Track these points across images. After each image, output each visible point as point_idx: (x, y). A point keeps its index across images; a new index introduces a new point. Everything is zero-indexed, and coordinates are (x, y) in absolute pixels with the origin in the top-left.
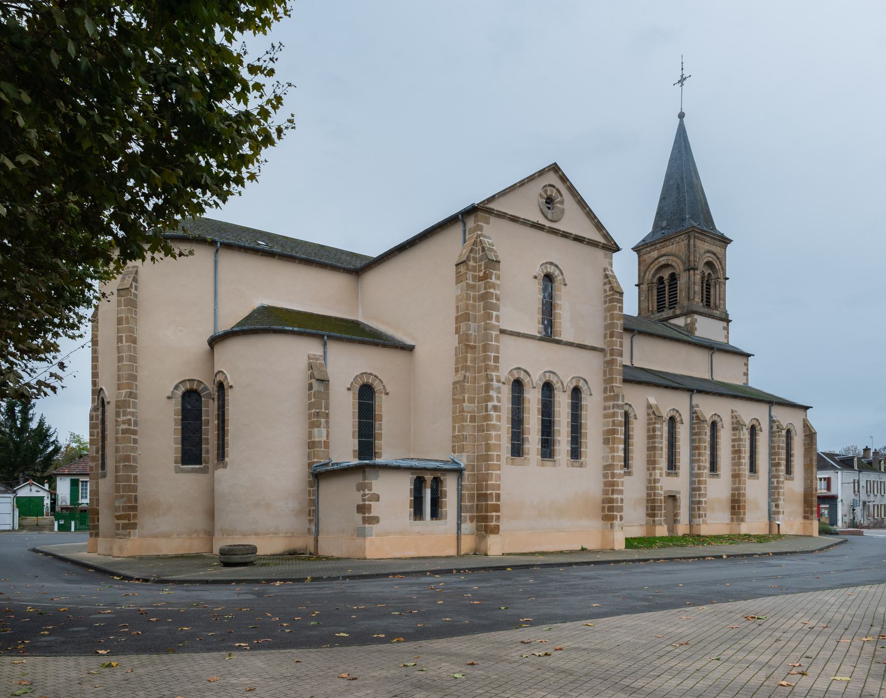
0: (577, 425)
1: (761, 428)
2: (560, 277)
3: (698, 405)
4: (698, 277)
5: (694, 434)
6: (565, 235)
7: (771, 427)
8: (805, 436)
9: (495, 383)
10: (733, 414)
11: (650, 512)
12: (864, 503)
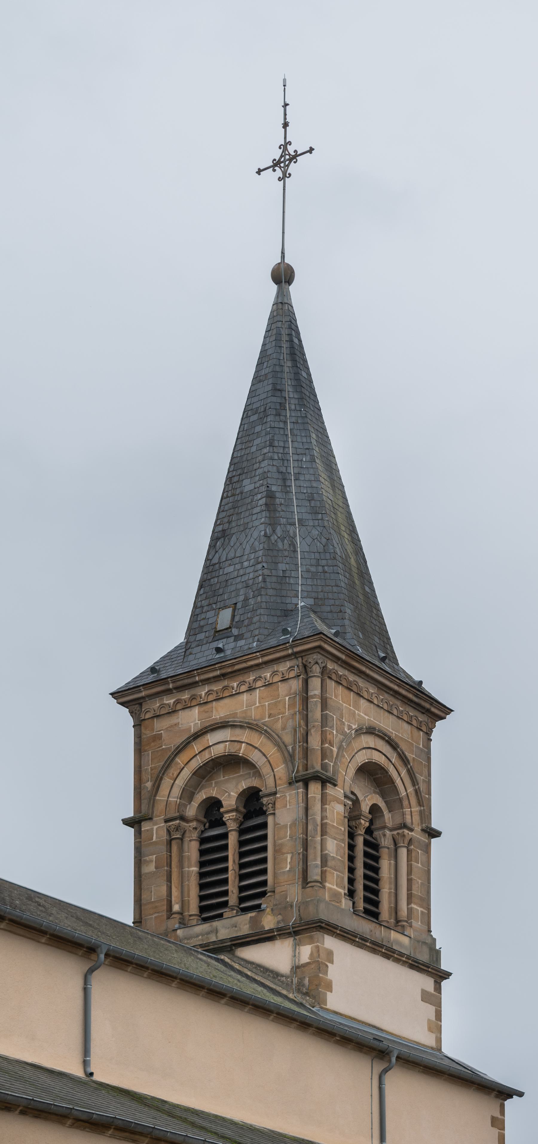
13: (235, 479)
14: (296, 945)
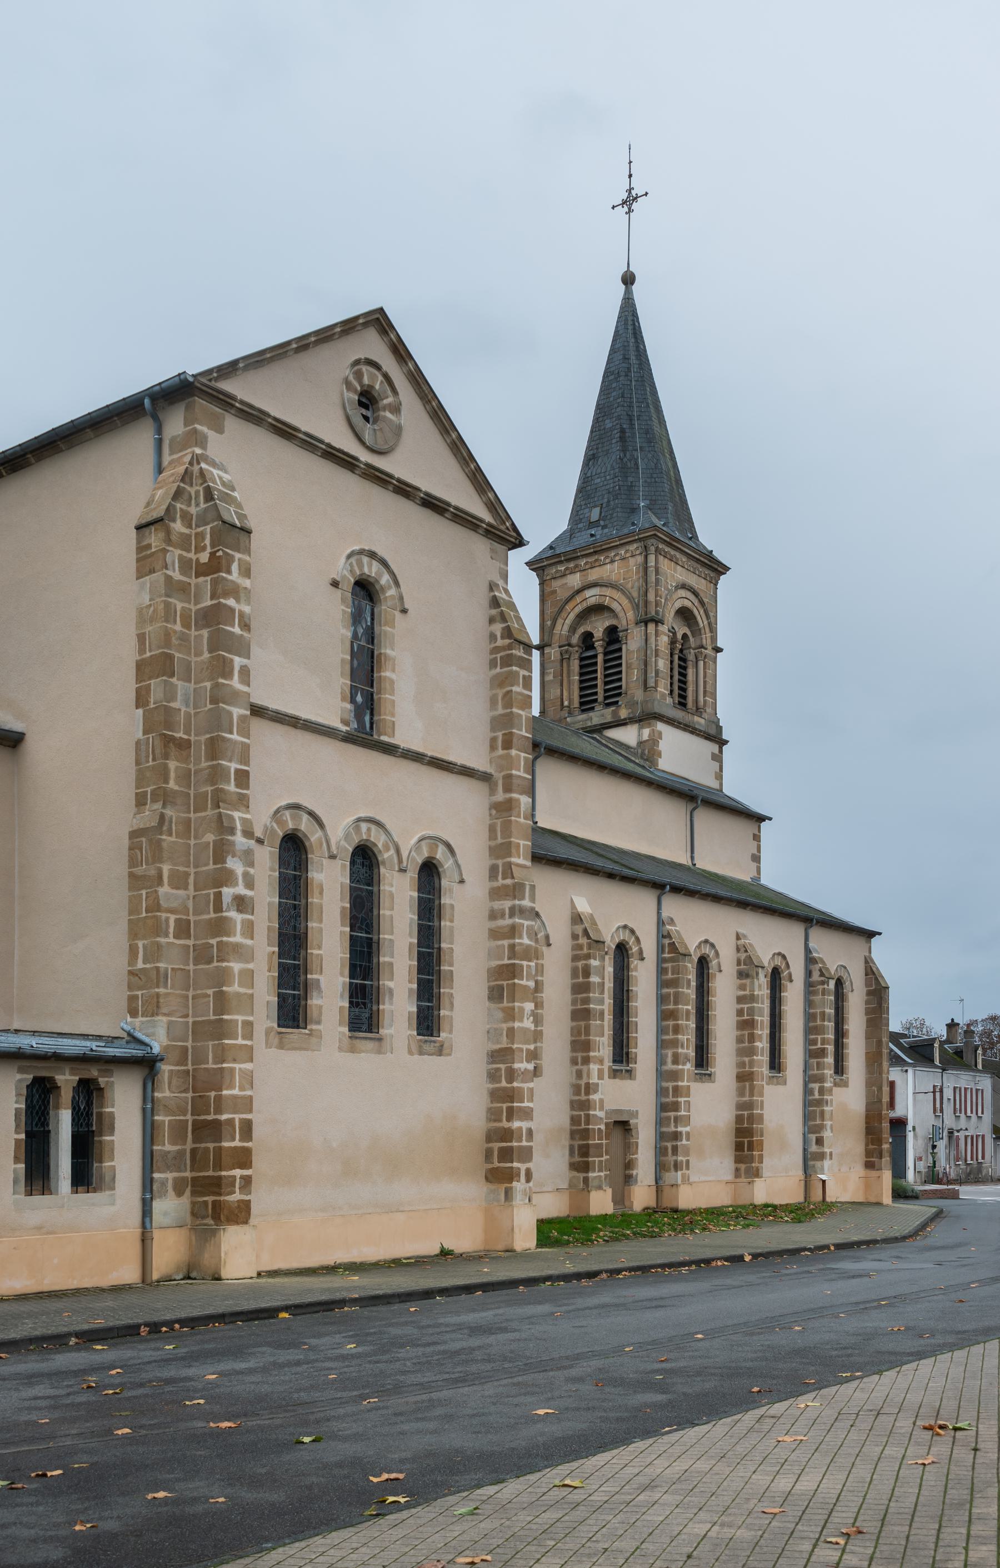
0: (430, 954)
1: (790, 975)
2: (392, 592)
3: (672, 919)
4: (664, 640)
5: (665, 982)
6: (404, 490)
7: (809, 973)
8: (869, 993)
9: (239, 839)
10: (739, 942)
11: (577, 1159)
12: (951, 1133)
13: (601, 419)
14: (641, 728)
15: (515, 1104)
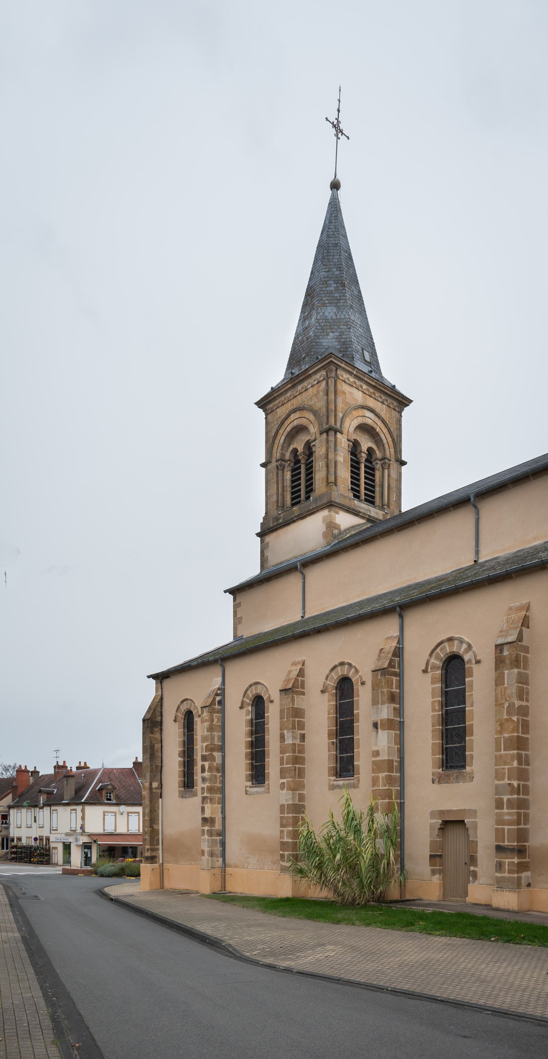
15: (516, 827)
